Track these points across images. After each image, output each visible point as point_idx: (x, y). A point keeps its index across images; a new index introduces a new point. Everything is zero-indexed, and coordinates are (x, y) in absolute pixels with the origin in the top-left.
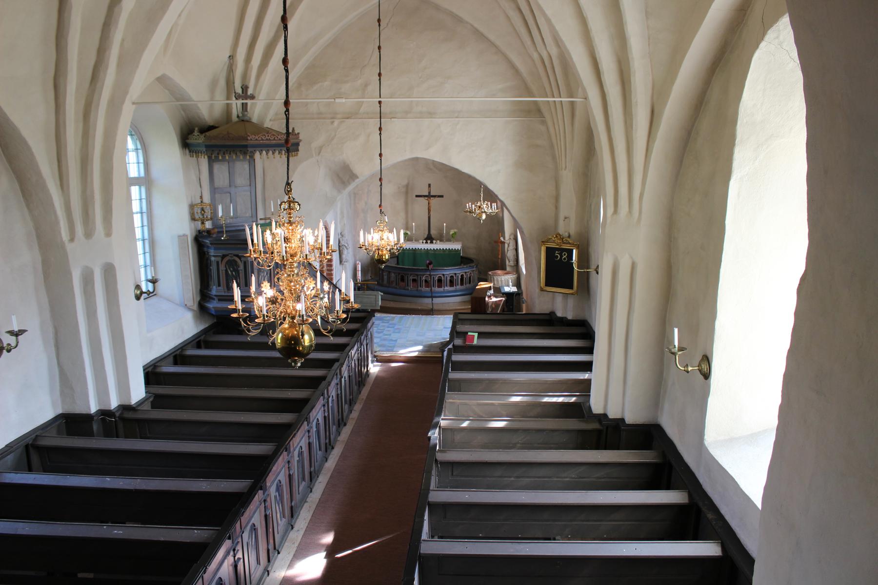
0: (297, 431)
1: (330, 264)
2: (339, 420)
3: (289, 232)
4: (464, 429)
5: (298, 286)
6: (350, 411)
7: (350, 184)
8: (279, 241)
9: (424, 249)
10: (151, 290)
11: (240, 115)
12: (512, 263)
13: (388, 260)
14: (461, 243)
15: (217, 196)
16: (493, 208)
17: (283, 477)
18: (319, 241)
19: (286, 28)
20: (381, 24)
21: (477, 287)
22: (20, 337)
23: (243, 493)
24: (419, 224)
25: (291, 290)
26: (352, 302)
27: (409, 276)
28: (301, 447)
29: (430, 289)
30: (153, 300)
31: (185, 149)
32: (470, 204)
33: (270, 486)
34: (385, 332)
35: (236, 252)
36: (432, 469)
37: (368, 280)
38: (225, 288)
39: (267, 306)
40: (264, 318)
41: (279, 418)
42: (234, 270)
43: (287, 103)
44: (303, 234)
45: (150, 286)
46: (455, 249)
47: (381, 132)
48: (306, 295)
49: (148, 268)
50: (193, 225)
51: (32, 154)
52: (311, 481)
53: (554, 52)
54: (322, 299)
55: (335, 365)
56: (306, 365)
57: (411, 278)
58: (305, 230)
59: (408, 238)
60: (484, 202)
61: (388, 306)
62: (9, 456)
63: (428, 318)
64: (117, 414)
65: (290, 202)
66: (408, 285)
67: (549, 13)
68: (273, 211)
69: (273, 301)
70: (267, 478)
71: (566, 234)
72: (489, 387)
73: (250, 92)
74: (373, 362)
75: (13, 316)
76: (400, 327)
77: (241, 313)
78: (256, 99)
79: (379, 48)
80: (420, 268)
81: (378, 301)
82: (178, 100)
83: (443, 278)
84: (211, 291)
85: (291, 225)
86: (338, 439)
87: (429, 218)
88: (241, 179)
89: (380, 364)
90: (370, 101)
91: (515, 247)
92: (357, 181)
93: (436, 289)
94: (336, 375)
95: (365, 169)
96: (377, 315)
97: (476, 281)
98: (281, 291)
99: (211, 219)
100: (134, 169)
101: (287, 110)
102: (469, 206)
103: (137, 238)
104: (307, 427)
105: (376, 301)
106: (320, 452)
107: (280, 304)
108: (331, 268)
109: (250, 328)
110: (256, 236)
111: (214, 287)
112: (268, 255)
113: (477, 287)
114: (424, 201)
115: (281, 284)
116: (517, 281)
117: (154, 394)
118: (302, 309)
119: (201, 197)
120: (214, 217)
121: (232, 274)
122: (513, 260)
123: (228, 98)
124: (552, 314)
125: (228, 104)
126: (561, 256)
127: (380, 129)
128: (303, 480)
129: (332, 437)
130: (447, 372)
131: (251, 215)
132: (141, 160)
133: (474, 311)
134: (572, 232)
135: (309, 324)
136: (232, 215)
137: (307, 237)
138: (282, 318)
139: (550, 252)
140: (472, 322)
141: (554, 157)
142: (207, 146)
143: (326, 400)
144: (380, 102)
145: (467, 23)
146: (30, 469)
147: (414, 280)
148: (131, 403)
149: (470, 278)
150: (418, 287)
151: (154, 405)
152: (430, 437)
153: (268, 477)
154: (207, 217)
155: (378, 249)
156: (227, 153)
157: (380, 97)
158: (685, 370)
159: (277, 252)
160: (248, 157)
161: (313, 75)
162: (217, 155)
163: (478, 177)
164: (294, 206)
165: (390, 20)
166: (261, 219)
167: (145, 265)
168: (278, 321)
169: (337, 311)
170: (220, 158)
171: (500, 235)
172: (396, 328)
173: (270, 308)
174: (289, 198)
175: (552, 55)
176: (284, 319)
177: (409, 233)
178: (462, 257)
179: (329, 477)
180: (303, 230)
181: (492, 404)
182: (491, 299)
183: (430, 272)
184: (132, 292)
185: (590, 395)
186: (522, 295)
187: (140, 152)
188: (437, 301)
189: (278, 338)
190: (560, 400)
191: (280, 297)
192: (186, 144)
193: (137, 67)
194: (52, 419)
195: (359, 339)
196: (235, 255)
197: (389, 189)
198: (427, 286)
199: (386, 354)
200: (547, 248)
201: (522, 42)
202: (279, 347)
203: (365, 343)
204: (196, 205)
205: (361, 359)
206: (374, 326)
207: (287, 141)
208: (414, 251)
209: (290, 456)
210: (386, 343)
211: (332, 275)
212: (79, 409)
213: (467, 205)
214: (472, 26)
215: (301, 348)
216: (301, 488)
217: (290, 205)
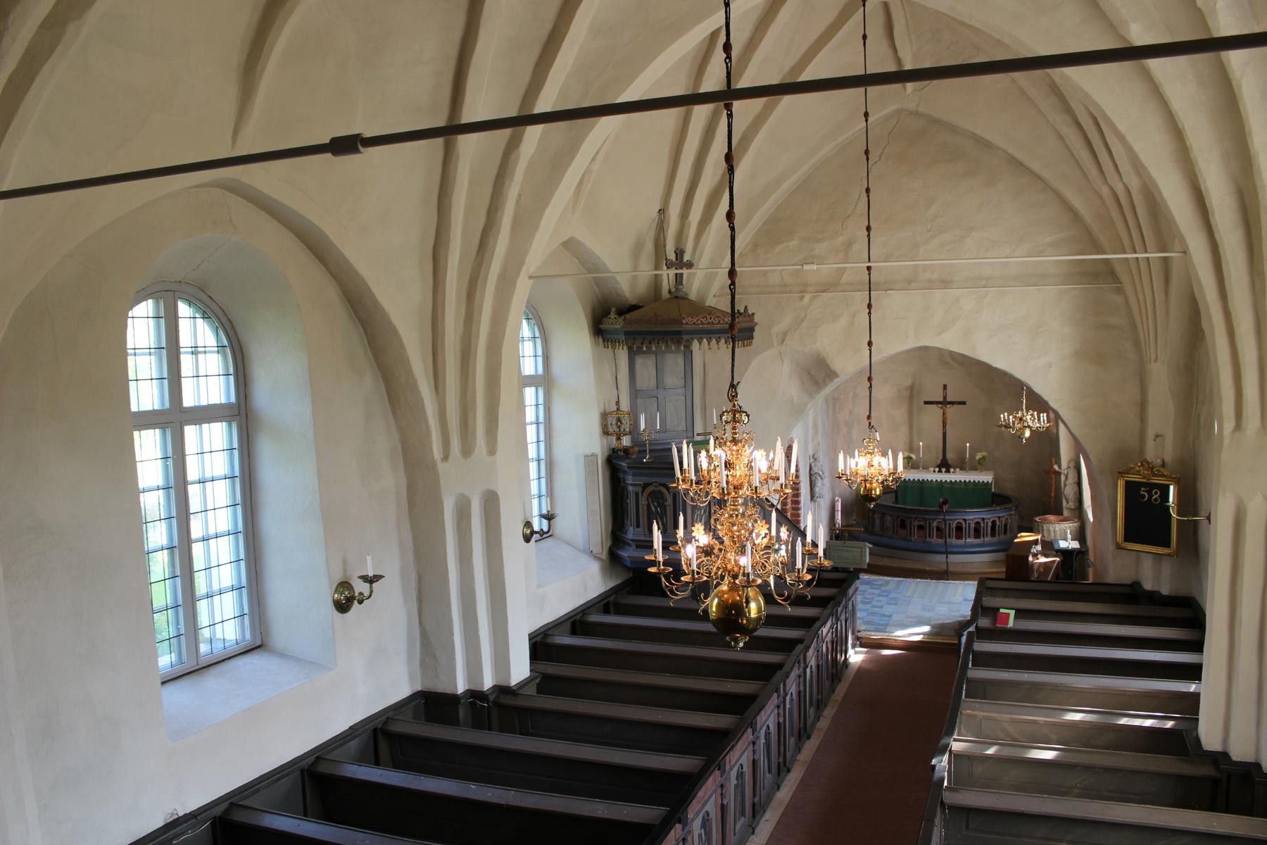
0: (737, 742)
1: (796, 501)
2: (800, 729)
3: (732, 455)
4: (989, 757)
5: (743, 531)
6: (817, 718)
7: (826, 385)
8: (718, 466)
9: (937, 481)
10: (545, 529)
11: (673, 290)
12: (1072, 505)
13: (879, 497)
14: (992, 472)
15: (639, 401)
16: (1042, 420)
17: (711, 807)
18: (776, 467)
20: (869, 156)
21: (1016, 540)
22: (374, 585)
23: (654, 825)
24: (928, 444)
25: (734, 537)
26: (820, 558)
28: (741, 765)
29: (944, 540)
30: (547, 543)
31: (598, 337)
32: (1006, 414)
33: (693, 820)
34: (874, 603)
35: (662, 480)
36: (934, 816)
37: (852, 526)
39: (697, 559)
40: (693, 575)
41: (712, 720)
43: (732, 273)
44: (753, 457)
45: (545, 522)
46: (983, 482)
48: (754, 544)
49: (543, 499)
50: (605, 440)
51: (402, 346)
52: (754, 816)
53: (1134, 183)
54: (777, 551)
55: (797, 648)
56: (752, 645)
57: (916, 523)
58: (756, 452)
59: (910, 464)
60: (1027, 411)
61: (881, 563)
62: (353, 742)
63: (940, 585)
64: (491, 698)
65: (734, 412)
67: (1122, 126)
68: (715, 423)
69: (707, 551)
70: (689, 807)
71: (1159, 461)
72: (1031, 695)
73: (687, 257)
74: (854, 646)
75: (368, 557)
76: (896, 595)
77: (662, 567)
78: (694, 268)
79: (868, 190)
80: (930, 509)
81: (865, 556)
82: (590, 271)
83: (964, 526)
84: (626, 533)
85: (736, 445)
86: (798, 758)
88: (673, 378)
89: (866, 650)
90: (855, 267)
91: (1076, 479)
92: (836, 380)
93: (954, 541)
94: (799, 662)
95: (848, 364)
96: (864, 577)
97: (1015, 528)
98: (720, 538)
99: (630, 433)
100: (530, 366)
101: (733, 283)
102: (1004, 417)
103: (530, 457)
104: (752, 737)
105: (862, 555)
106: (770, 775)
107: (718, 557)
108: (797, 506)
109: (674, 588)
110: (686, 458)
111: (631, 528)
112: (702, 487)
113: (1016, 540)
114: (936, 411)
115: (719, 527)
116: (1080, 534)
117: (541, 673)
118: (748, 564)
119: (618, 403)
120: (634, 431)
121: (656, 510)
122: (1073, 500)
123: (657, 267)
124: (1136, 585)
125: (656, 276)
126: (1150, 496)
127: (869, 306)
128: (742, 815)
129: (789, 754)
130: (965, 668)
131: (685, 429)
132: (540, 352)
133: (1010, 576)
134: (1168, 458)
135: (757, 586)
136: (658, 427)
137: (758, 463)
138: (719, 577)
140: (1006, 592)
141: (1137, 344)
142: (627, 333)
143: (781, 699)
144: (869, 268)
145: (998, 148)
146: (377, 763)
147: (920, 527)
148: (510, 684)
149: (1006, 525)
150: (926, 538)
151: (541, 690)
152: (934, 766)
153: (691, 805)
155: (865, 481)
156: (654, 343)
157: (869, 261)
159: (716, 482)
160: (682, 348)
161: (774, 231)
162: (640, 345)
163: (1019, 374)
164: (741, 418)
165: (883, 150)
166: (698, 435)
167: (540, 494)
168: (713, 580)
169: (799, 569)
170: (644, 349)
171: (1054, 463)
172: (890, 596)
173: (703, 561)
174: (734, 406)
175: (1130, 189)
176: (722, 578)
177: (913, 456)
178: (994, 494)
179: (780, 814)
180: (753, 451)
181: (1035, 722)
182: (1038, 559)
183: (944, 516)
184: (519, 530)
185: (1198, 719)
186: (1088, 555)
187: (539, 341)
188: (954, 558)
189: (713, 604)
190: (1148, 723)
191: (717, 546)
192: (598, 330)
193: (537, 228)
194: (408, 697)
195: (835, 610)
196: (661, 485)
197: (883, 392)
198: (939, 536)
199: (876, 636)
200: (1127, 482)
201: (1083, 171)
202: (714, 618)
203: (843, 618)
204: (611, 413)
205: (837, 640)
206: (858, 592)
207: (732, 326)
208: (922, 483)
209: (724, 777)
210: (875, 619)
211: (798, 515)
212: (442, 687)
213: (1002, 416)
214: (1005, 152)
215: (745, 622)
216: (738, 827)
217: (735, 415)
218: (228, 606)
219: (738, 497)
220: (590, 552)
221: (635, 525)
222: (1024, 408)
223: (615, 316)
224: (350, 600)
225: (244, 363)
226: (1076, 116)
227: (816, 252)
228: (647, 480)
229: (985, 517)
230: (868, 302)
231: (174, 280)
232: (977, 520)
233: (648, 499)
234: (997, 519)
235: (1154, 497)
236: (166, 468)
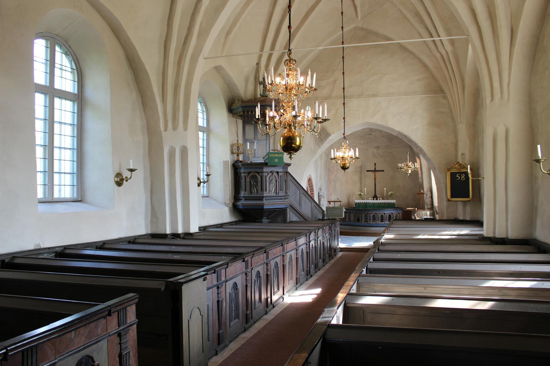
9: (372, 203)
19: (290, 10)
22: (133, 173)
26: (326, 117)
27: (362, 214)
31: (230, 113)
35: (257, 170)
42: (255, 181)
46: (392, 203)
47: (344, 90)
50: (232, 156)
60: (409, 162)
66: (362, 220)
80: (369, 209)
87: (375, 184)
91: (430, 195)
100: (202, 122)
106: (303, 272)
114: (372, 174)
121: (254, 183)
122: (429, 204)
126: (461, 177)
132: (205, 118)
139: (453, 175)
148: (190, 231)
154: (240, 152)
158: (548, 173)
187: (205, 113)
192: (231, 110)
196: (256, 172)
200: (451, 173)
208: (366, 204)
212: (160, 231)
218: (67, 180)
219: (291, 94)
221: (244, 191)
222: (408, 161)
223: (238, 101)
224: (122, 180)
225: (82, 78)
226: (426, 24)
229: (393, 212)
230: (343, 87)
231: (55, 34)
232: (389, 214)
234: (398, 214)
235: (462, 178)
236: (45, 112)
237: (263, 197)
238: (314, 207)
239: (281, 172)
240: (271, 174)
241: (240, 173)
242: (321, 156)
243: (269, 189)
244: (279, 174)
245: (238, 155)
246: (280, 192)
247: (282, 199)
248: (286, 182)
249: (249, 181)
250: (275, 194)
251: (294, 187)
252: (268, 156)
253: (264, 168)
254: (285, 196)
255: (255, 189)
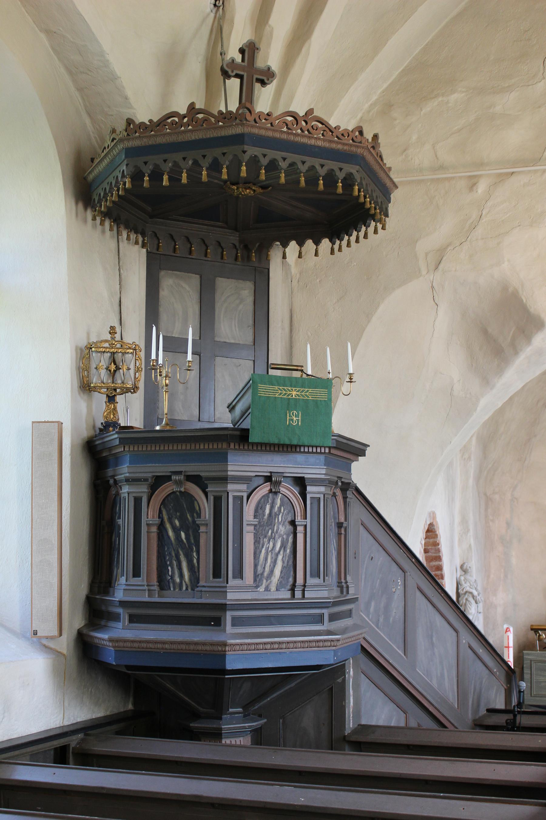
7: (516, 353)
31: (86, 208)
35: (193, 468)
38: (155, 581)
42: (185, 526)
121: (178, 537)
220: (29, 634)
227: (498, 109)
228: (162, 469)
233: (160, 512)
237: (223, 607)
238: (470, 651)
239: (317, 482)
240: (265, 489)
241: (115, 482)
242: (465, 449)
243: (256, 566)
244: (309, 488)
245: (111, 399)
246: (311, 581)
247: (320, 619)
248: (340, 534)
249: (157, 521)
250: (288, 595)
251: (381, 558)
252: (254, 394)
253: (231, 457)
254: (335, 604)
255: (184, 565)
